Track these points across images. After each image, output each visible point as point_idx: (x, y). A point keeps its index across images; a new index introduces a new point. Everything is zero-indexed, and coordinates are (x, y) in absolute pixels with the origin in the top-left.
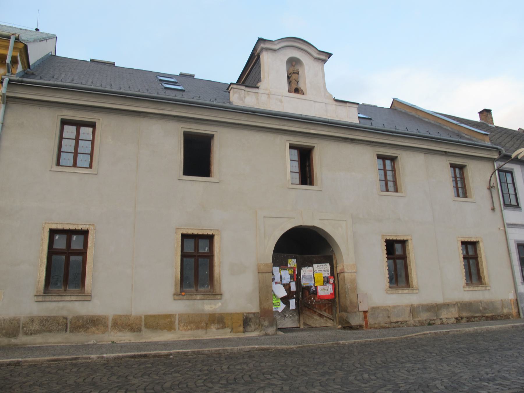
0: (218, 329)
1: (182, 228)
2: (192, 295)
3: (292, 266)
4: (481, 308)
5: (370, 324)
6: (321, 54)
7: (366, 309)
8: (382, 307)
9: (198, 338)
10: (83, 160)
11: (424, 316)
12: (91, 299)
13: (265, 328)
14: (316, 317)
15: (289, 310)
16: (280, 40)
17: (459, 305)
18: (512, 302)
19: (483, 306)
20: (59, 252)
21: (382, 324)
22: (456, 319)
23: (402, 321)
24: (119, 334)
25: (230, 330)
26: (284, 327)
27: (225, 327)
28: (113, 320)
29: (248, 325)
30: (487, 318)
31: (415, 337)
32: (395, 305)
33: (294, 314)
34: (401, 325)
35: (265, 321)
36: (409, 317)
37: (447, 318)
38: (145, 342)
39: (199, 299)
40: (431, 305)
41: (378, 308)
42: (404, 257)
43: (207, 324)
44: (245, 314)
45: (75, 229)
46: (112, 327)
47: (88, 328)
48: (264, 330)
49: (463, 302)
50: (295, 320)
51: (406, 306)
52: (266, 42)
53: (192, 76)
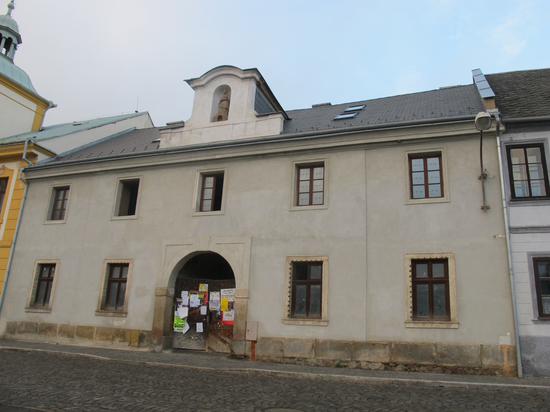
0: (120, 342)
1: (108, 258)
2: (107, 312)
3: (204, 290)
4: (435, 354)
5: (258, 356)
6: (246, 73)
7: (254, 339)
8: (275, 338)
9: (106, 348)
10: (434, 190)
11: (332, 355)
12: (51, 312)
13: (153, 345)
14: (220, 343)
15: (196, 333)
16: (206, 75)
17: (393, 346)
18: (505, 351)
19: (439, 351)
20: (115, 281)
21: (273, 358)
22: (386, 364)
23: (300, 357)
24: (62, 338)
25: (128, 344)
26: (188, 348)
27: (125, 341)
28: (60, 327)
29: (142, 341)
30: (444, 370)
31: (228, 371)
32: (292, 337)
33: (201, 337)
34: (297, 363)
35: (154, 339)
36: (309, 353)
37: (368, 362)
38: (75, 346)
39: (110, 316)
40: (345, 342)
41: (269, 339)
42: (50, 280)
43: (113, 337)
44: (141, 332)
45: (424, 258)
46: (59, 332)
47: (47, 332)
48: (153, 347)
49: (401, 343)
50: (201, 343)
51: (308, 341)
52: (194, 81)
53: (329, 104)
